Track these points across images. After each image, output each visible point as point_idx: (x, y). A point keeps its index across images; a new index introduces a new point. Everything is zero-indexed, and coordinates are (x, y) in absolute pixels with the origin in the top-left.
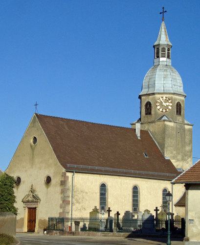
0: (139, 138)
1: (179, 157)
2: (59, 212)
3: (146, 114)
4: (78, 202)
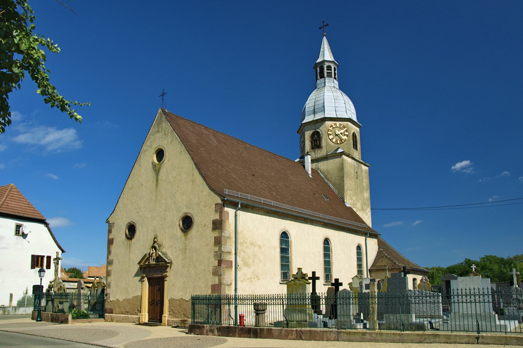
0: (311, 176)
2: (210, 284)
4: (246, 264)
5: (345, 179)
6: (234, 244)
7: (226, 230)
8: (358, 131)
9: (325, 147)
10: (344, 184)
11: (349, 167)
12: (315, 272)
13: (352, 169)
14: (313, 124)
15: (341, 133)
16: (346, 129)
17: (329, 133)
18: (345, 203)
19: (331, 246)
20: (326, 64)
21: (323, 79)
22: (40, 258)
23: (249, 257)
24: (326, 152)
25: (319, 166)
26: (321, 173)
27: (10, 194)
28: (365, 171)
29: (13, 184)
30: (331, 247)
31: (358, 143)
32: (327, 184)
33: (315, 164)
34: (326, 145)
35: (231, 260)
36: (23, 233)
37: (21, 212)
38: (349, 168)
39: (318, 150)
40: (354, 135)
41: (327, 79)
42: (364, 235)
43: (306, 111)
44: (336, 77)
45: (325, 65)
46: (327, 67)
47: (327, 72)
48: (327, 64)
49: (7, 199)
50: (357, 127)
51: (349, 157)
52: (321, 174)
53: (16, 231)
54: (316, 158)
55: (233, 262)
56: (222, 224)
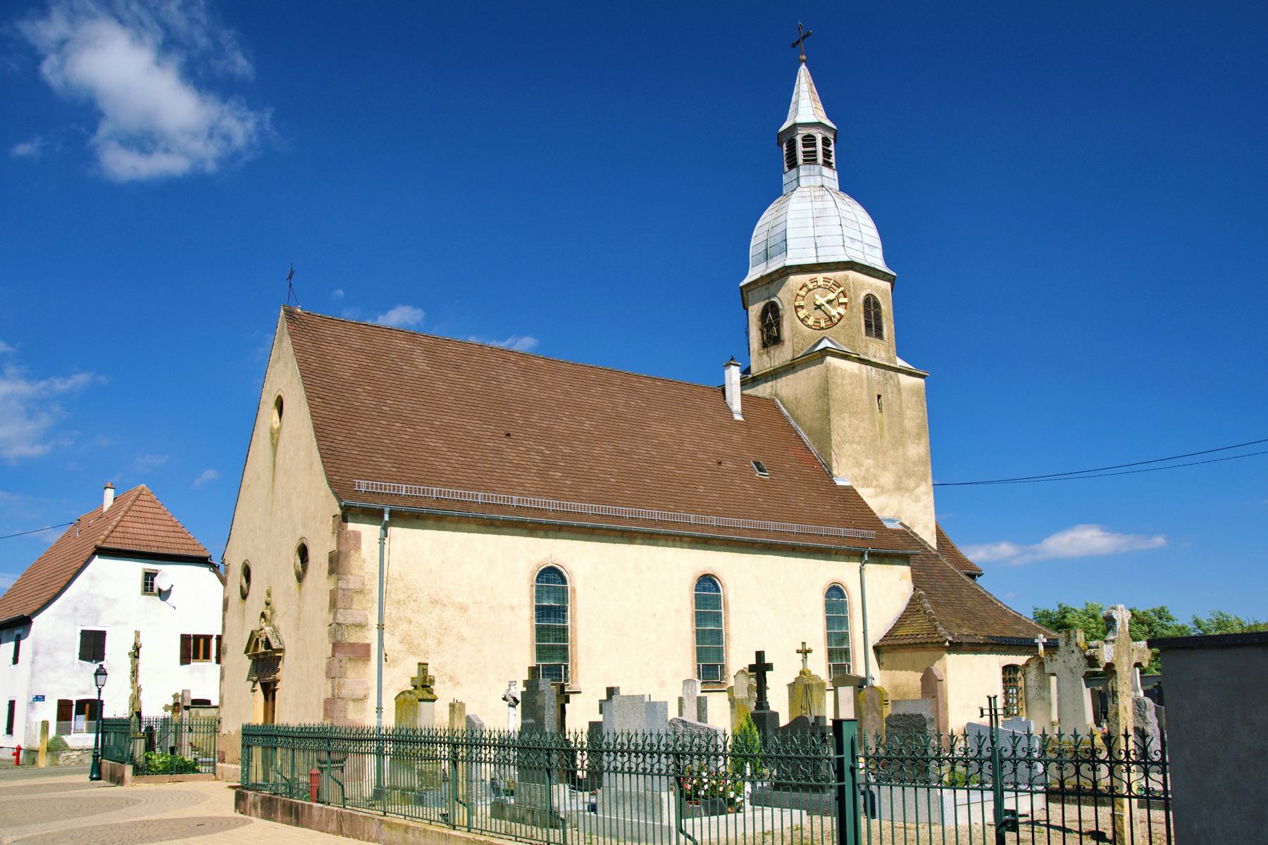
0: (738, 417)
1: (887, 479)
3: (765, 345)
5: (833, 416)
6: (376, 606)
7: (352, 574)
8: (887, 291)
9: (789, 340)
10: (830, 429)
11: (851, 384)
12: (764, 652)
13: (862, 388)
14: (763, 286)
15: (829, 302)
16: (842, 289)
17: (797, 304)
18: (834, 478)
19: (724, 593)
20: (799, 132)
21: (795, 170)
22: (202, 641)
23: (425, 633)
24: (792, 351)
25: (779, 388)
26: (781, 406)
27: (134, 508)
28: (915, 392)
29: (144, 485)
30: (724, 596)
31: (884, 320)
32: (796, 432)
33: (770, 383)
34: (791, 335)
35: (367, 642)
36: (160, 590)
37: (152, 544)
38: (848, 388)
39: (774, 349)
40: (871, 305)
41: (803, 169)
42: (856, 558)
43: (750, 256)
44: (833, 160)
45: (799, 135)
46: (803, 140)
47: (804, 152)
48: (802, 132)
49: (126, 519)
50: (882, 279)
51: (849, 360)
52: (783, 409)
53: (143, 585)
54: (771, 369)
55: (372, 646)
56: (340, 561)
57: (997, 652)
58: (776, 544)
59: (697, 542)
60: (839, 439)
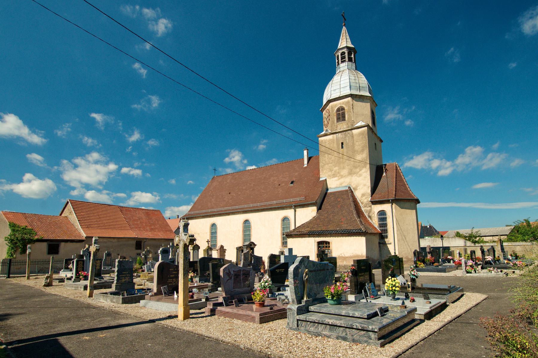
51: (328, 135)
57: (314, 237)
58: (264, 209)
59: (244, 212)
60: (323, 164)
